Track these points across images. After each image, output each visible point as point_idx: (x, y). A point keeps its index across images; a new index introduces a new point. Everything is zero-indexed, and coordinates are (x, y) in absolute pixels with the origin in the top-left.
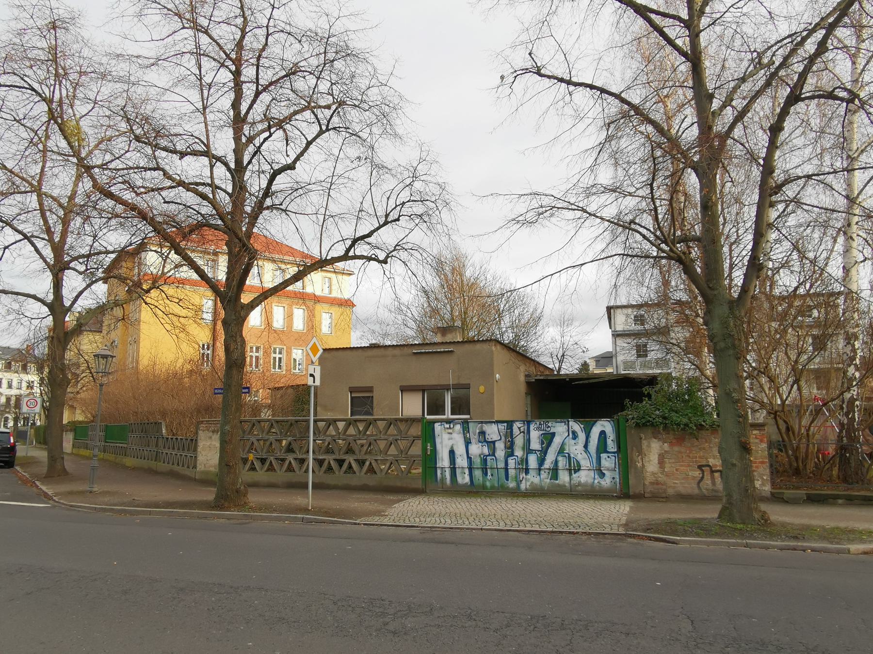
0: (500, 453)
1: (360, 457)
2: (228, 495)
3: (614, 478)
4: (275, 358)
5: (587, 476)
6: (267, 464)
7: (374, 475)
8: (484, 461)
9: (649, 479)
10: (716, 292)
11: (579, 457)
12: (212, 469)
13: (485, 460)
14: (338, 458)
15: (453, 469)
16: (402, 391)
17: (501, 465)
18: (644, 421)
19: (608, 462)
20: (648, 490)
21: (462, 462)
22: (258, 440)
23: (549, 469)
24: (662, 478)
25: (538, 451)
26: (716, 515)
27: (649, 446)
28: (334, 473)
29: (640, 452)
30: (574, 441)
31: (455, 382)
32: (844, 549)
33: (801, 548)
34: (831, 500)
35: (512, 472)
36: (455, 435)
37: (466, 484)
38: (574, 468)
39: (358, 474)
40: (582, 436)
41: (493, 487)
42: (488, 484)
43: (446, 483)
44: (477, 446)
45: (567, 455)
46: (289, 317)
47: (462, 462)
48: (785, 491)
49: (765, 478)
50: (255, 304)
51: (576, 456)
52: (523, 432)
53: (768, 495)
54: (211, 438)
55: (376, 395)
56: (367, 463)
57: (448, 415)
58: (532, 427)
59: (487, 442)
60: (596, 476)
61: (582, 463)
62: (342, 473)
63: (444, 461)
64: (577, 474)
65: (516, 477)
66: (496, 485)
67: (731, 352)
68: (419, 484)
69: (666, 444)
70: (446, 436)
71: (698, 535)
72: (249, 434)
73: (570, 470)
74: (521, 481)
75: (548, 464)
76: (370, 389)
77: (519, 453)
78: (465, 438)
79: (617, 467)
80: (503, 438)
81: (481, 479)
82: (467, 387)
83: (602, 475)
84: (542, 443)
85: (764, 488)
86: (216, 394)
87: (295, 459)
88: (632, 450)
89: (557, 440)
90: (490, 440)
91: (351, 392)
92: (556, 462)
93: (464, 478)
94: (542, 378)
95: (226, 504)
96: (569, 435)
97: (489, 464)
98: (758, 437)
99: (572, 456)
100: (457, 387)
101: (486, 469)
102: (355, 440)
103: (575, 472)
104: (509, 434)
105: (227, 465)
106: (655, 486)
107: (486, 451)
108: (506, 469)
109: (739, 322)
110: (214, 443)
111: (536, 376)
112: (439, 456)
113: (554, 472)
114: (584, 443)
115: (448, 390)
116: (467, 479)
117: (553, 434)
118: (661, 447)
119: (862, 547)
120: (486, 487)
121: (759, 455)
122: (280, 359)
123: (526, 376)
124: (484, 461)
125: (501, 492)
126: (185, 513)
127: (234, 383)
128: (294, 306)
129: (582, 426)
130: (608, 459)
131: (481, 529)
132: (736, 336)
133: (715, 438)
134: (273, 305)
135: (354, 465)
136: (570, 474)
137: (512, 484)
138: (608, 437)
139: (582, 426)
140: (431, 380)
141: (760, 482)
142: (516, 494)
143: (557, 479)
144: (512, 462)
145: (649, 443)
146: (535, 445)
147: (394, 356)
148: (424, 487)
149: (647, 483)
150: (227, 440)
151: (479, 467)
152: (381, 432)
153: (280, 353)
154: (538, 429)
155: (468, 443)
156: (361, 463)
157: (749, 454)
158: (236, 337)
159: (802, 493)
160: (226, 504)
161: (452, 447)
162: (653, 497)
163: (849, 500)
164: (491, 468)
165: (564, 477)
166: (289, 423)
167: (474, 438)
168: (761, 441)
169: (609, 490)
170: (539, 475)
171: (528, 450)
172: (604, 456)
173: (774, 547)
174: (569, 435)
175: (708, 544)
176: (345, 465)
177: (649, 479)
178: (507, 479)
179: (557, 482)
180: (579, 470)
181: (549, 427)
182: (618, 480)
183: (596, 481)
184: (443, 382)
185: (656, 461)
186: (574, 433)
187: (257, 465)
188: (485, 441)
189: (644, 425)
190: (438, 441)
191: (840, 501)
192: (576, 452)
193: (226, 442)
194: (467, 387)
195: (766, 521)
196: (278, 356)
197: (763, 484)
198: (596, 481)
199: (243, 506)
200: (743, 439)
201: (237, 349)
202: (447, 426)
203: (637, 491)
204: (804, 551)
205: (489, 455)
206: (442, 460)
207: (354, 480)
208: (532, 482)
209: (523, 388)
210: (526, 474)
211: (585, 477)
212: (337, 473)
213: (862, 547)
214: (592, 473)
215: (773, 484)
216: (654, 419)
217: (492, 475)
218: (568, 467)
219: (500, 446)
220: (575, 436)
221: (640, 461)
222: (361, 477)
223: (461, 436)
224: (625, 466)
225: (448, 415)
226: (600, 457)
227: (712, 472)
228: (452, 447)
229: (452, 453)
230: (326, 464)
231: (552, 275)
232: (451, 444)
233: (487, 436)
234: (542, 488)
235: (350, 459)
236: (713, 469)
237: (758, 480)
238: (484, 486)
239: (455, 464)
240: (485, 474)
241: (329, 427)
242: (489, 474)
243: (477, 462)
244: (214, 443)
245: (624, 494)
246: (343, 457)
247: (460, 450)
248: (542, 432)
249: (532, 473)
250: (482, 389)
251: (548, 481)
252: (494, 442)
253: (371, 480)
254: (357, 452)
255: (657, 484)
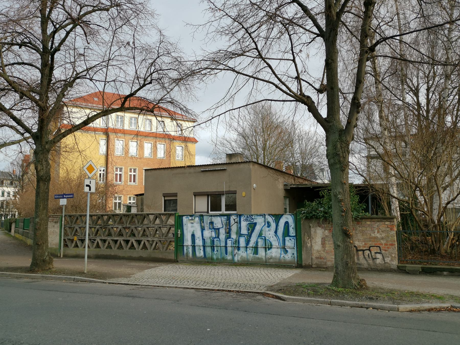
0: (223, 236)
1: (138, 239)
2: (37, 263)
3: (293, 254)
4: (100, 174)
5: (276, 252)
6: (74, 242)
7: (147, 251)
8: (213, 242)
9: (315, 255)
10: (331, 124)
11: (271, 240)
12: (54, 246)
13: (213, 241)
14: (125, 239)
15: (194, 247)
16: (195, 196)
17: (223, 244)
18: (311, 215)
19: (290, 243)
20: (314, 263)
21: (199, 242)
22: (80, 228)
23: (253, 247)
24: (324, 254)
25: (246, 235)
26: (330, 281)
27: (315, 232)
28: (123, 249)
29: (310, 236)
30: (268, 229)
31: (228, 190)
32: (395, 308)
33: (366, 306)
34: (439, 272)
35: (229, 249)
36: (195, 224)
37: (202, 256)
38: (268, 247)
39: (137, 249)
40: (273, 225)
41: (217, 259)
42: (215, 257)
43: (189, 256)
44: (209, 231)
45: (264, 238)
46: (154, 149)
47: (199, 242)
48: (407, 265)
49: (393, 255)
50: (56, 140)
51: (270, 238)
52: (237, 222)
53: (395, 267)
54: (54, 226)
55: (178, 198)
56: (142, 243)
57: (223, 211)
58: (242, 219)
59: (215, 229)
60: (282, 253)
61: (274, 243)
62: (127, 249)
63: (188, 241)
64: (270, 251)
65: (232, 252)
66: (220, 257)
67: (338, 166)
68: (172, 256)
69: (326, 231)
70: (189, 225)
71: (309, 295)
72: (75, 223)
73: (266, 248)
74: (235, 255)
75: (252, 244)
76: (175, 195)
77: (234, 236)
78: (201, 226)
79: (295, 246)
80: (224, 226)
81: (210, 253)
82: (235, 193)
83: (286, 252)
84: (249, 230)
85: (392, 263)
86: (55, 198)
87: (124, 240)
88: (305, 235)
89: (258, 228)
90: (216, 228)
91: (164, 197)
92: (257, 243)
93: (200, 253)
94: (295, 186)
95: (36, 269)
96: (265, 224)
97: (215, 243)
98: (389, 226)
99: (267, 238)
100: (228, 193)
101: (214, 247)
102: (160, 228)
103: (269, 250)
104: (228, 223)
105: (37, 244)
106: (320, 260)
107: (214, 235)
108: (226, 247)
109: (344, 145)
110: (55, 230)
111: (291, 185)
112: (185, 238)
113: (256, 249)
114: (275, 229)
115: (223, 194)
116: (202, 254)
117: (255, 224)
118: (323, 233)
119: (410, 306)
120: (214, 259)
121: (390, 239)
122: (134, 176)
123: (285, 185)
124: (213, 242)
125: (222, 262)
126: (10, 275)
127: (41, 191)
128: (145, 142)
129: (274, 218)
130: (289, 240)
131: (176, 287)
132: (341, 155)
133: (359, 227)
134: (158, 143)
135: (135, 244)
136: (266, 251)
137: (229, 257)
138: (290, 226)
139: (274, 218)
140: (213, 188)
141: (390, 259)
142: (233, 264)
143: (257, 254)
144: (229, 243)
145: (315, 230)
146: (244, 231)
147: (190, 173)
148: (176, 258)
149: (314, 257)
150: (37, 228)
151: (209, 245)
152: (150, 222)
153: (135, 172)
154: (246, 220)
155: (203, 229)
156: (139, 242)
157: (350, 238)
158: (42, 162)
159: (418, 267)
160: (36, 269)
161: (193, 232)
162: (318, 267)
163: (451, 272)
164: (217, 246)
165: (262, 253)
166: (131, 216)
167: (207, 226)
168: (392, 229)
169: (290, 262)
170: (246, 251)
171: (239, 234)
172: (287, 238)
173: (348, 305)
174: (265, 224)
175: (304, 301)
176: (130, 244)
177: (315, 255)
178: (226, 254)
179: (257, 256)
180: (271, 248)
181: (253, 219)
182: (296, 255)
183: (282, 256)
184: (220, 190)
185: (320, 243)
186: (268, 223)
187: (112, 244)
188: (213, 228)
189: (312, 218)
190: (185, 228)
191: (445, 273)
192: (270, 236)
193: (36, 229)
194: (235, 193)
195: (361, 286)
196: (133, 173)
197: (392, 260)
198: (282, 256)
199: (49, 270)
200: (344, 228)
201: (42, 169)
202: (190, 218)
203: (307, 263)
204: (367, 308)
205: (215, 238)
206: (187, 241)
207: (134, 254)
208: (242, 256)
209: (281, 193)
210: (238, 250)
211: (275, 253)
212: (125, 249)
213: (410, 306)
214: (279, 250)
215: (400, 261)
216: (318, 213)
217: (217, 251)
218: (264, 246)
219: (222, 231)
220: (269, 225)
221: (310, 242)
222: (138, 252)
223: (199, 224)
224: (300, 245)
225: (223, 211)
226: (285, 239)
227: (357, 251)
228: (193, 232)
229: (193, 236)
230: (118, 242)
231: (219, 115)
232: (192, 230)
233: (214, 225)
234: (248, 260)
235: (133, 240)
236: (358, 249)
237: (388, 257)
238: (212, 259)
239: (195, 244)
240: (213, 250)
241: (156, 219)
242: (215, 250)
243: (208, 242)
244: (55, 230)
245: (299, 266)
246: (128, 239)
247: (198, 234)
248: (248, 222)
249: (242, 250)
250: (244, 194)
251: (252, 255)
252: (218, 229)
253: (144, 254)
254: (136, 235)
255: (321, 258)
